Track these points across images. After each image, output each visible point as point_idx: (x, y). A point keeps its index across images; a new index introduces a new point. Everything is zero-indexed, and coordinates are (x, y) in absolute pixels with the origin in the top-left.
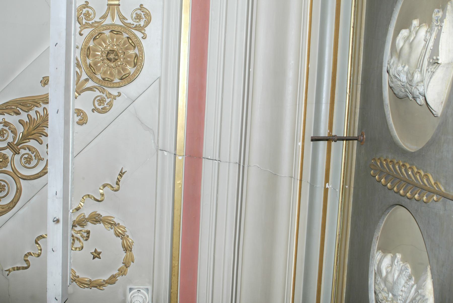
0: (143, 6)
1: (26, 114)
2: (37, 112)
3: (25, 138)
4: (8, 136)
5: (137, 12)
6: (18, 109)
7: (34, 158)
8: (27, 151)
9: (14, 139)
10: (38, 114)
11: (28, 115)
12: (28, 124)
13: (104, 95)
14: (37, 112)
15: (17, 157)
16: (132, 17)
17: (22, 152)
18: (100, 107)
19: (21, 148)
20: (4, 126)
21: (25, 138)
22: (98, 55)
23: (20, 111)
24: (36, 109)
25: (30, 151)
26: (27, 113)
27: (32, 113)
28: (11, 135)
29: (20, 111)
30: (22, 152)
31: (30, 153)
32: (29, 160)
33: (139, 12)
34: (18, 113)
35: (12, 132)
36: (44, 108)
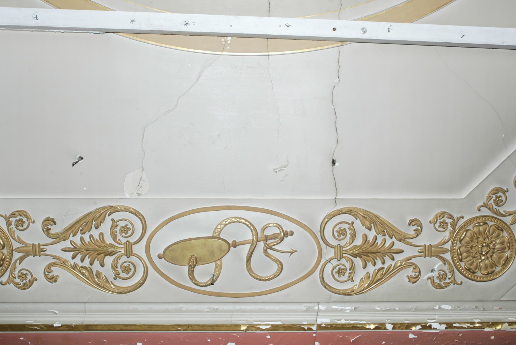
18: (500, 194)
29: (373, 228)
34: (98, 274)
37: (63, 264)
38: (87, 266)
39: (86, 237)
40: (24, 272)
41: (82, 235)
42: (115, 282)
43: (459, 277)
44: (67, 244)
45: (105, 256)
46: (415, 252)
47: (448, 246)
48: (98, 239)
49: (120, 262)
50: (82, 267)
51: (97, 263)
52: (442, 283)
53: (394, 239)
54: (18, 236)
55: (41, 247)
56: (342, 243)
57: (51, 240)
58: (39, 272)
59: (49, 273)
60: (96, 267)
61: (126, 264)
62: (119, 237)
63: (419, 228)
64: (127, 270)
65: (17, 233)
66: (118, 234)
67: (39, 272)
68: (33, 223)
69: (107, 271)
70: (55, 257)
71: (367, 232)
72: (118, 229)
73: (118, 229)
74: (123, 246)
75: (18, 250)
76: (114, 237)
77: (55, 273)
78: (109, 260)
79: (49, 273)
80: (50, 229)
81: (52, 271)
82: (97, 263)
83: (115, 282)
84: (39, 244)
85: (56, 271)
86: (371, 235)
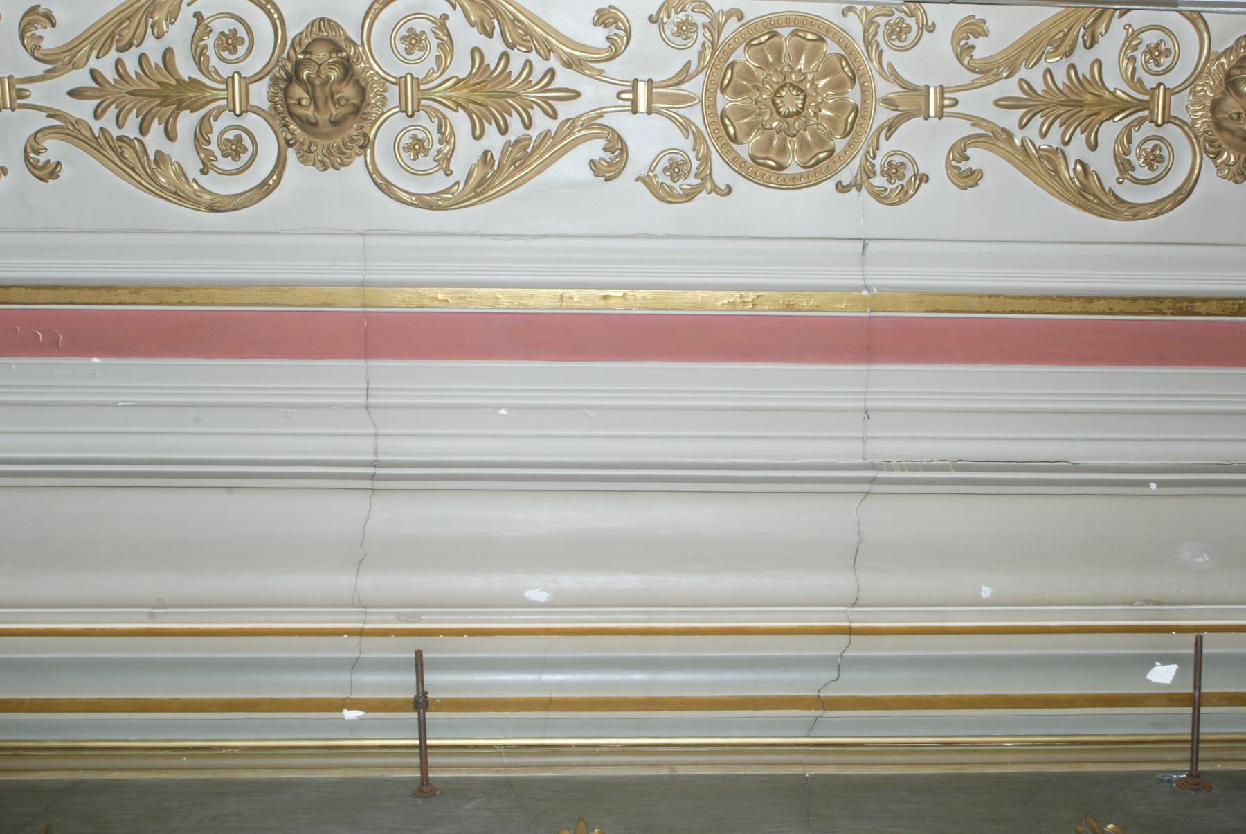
0: (654, 13)
1: (503, 48)
2: (528, 63)
3: (1120, 107)
4: (1146, 140)
5: (909, 165)
6: (495, 21)
7: (1142, 48)
8: (433, 127)
9: (1140, 122)
10: (503, 62)
11: (505, 55)
12: (1084, 124)
13: (437, 146)
14: (528, 63)
15: (399, 121)
16: (895, 153)
17: (1150, 82)
19: (1145, 92)
20: (1133, 169)
21: (1120, 107)
22: (830, 109)
23: (497, 31)
24: (533, 56)
25: (440, 131)
26: (1065, 149)
27: (518, 59)
28: (1137, 137)
29: (497, 31)
30: (422, 119)
31: (436, 136)
32: (418, 147)
33: (669, 30)
35: (1130, 142)
36: (1022, 127)
37: (70, 130)
38: (132, 137)
39: (131, 61)
40: (897, 160)
41: (121, 55)
42: (203, 180)
43: (722, 173)
44: (1010, 88)
45: (179, 108)
46: (37, 94)
47: (695, 86)
48: (161, 65)
49: (217, 126)
50: (120, 139)
51: (156, 128)
52: (676, 186)
53: (554, 62)
54: (890, 65)
55: (18, 86)
56: (420, 71)
57: (40, 68)
58: (933, 161)
59: (38, 153)
60: (155, 140)
61: (230, 135)
62: (214, 61)
63: (622, 33)
64: (234, 149)
65: (889, 56)
66: (211, 52)
67: (933, 161)
68: (931, 31)
69: (182, 152)
70: (976, 121)
71: (479, 40)
72: (210, 41)
73: (210, 41)
74: (224, 86)
75: (889, 102)
76: (199, 58)
77: (973, 164)
78: (187, 122)
79: (38, 153)
80: (973, 47)
81: (967, 158)
82: (156, 128)
83: (203, 180)
84: (10, 77)
85: (978, 157)
86: (493, 48)
